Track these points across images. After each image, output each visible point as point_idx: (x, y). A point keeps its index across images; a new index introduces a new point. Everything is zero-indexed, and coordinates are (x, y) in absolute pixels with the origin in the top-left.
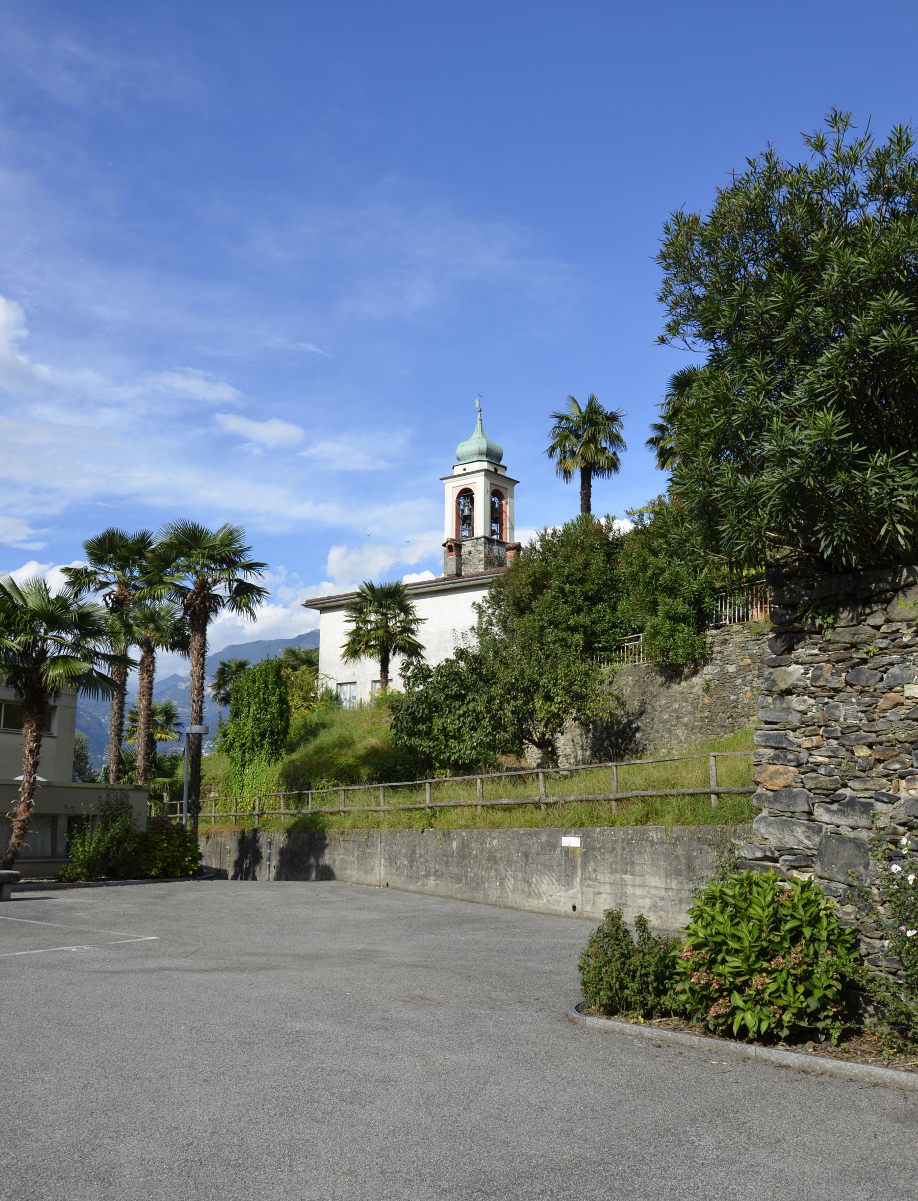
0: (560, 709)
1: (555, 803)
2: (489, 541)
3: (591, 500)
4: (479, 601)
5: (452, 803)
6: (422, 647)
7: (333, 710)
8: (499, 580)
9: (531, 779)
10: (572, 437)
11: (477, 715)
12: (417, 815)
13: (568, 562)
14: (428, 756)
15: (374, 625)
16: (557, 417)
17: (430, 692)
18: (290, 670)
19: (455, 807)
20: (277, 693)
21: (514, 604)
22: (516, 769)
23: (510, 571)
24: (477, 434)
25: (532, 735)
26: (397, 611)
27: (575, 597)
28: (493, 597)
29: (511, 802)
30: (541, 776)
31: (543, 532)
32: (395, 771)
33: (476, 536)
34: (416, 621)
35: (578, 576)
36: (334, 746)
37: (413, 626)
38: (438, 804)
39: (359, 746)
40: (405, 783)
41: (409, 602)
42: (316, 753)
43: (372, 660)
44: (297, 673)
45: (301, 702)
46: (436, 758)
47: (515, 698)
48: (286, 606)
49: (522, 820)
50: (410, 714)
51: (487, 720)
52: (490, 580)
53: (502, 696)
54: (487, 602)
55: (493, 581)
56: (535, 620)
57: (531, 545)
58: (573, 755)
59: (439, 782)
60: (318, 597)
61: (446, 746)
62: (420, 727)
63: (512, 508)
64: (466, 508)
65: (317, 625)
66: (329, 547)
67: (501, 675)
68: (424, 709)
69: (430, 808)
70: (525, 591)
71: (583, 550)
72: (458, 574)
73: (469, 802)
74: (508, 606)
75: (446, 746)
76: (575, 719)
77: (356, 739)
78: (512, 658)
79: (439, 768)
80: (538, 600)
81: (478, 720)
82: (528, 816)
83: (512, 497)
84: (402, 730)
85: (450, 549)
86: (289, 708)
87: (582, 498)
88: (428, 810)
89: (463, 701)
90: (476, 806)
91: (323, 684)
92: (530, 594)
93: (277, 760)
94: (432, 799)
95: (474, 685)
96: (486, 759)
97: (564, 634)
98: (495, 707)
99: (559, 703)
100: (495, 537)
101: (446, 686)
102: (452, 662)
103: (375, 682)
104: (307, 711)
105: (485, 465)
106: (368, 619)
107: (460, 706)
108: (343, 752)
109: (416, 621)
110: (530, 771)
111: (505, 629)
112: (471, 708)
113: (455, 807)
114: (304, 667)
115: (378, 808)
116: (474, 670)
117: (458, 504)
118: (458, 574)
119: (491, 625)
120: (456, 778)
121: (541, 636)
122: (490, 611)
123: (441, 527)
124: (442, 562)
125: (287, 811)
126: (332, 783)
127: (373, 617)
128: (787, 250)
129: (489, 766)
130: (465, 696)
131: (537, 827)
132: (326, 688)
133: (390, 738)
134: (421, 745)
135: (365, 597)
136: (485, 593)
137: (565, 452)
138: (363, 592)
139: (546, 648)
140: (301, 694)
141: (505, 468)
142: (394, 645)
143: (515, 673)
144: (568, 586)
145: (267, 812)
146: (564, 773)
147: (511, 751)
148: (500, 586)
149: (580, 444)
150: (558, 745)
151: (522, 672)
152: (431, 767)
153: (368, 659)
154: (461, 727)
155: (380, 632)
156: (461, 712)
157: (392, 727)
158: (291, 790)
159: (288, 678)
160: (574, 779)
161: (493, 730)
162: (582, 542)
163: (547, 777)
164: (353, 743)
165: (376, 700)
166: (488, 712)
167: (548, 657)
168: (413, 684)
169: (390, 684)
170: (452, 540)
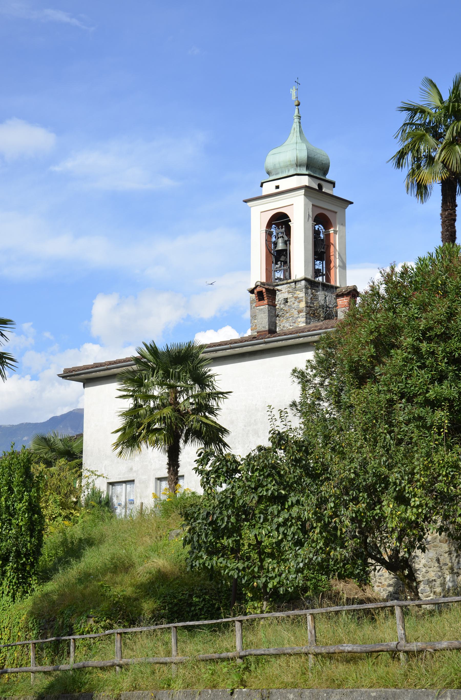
0: (418, 515)
1: (420, 651)
3: (457, 224)
4: (302, 366)
5: (272, 651)
6: (224, 431)
7: (103, 520)
8: (328, 338)
9: (382, 615)
10: (429, 137)
11: (303, 525)
12: (223, 668)
13: (425, 311)
14: (236, 583)
15: (158, 401)
16: (408, 109)
17: (238, 492)
18: (42, 466)
19: (277, 656)
20: (26, 498)
21: (351, 371)
22: (361, 602)
23: (343, 325)
24: (294, 136)
25: (380, 553)
26: (190, 382)
27: (436, 360)
28: (320, 362)
29: (357, 648)
30: (398, 611)
31: (388, 270)
32: (191, 605)
33: (293, 278)
34: (217, 395)
35: (439, 330)
36: (105, 571)
37: (212, 403)
38: (253, 652)
39: (140, 569)
40: (206, 622)
41: (206, 369)
42: (80, 581)
43: (156, 450)
44: (52, 469)
45: (58, 510)
46: (247, 585)
47: (355, 500)
48: (35, 378)
49: (374, 677)
50: (210, 524)
51: (318, 530)
52: (316, 338)
53: (337, 498)
54: (313, 367)
55: (321, 339)
56: (379, 392)
57: (373, 288)
58: (438, 582)
59: (253, 620)
60: (81, 364)
61: (261, 568)
62: (225, 541)
63: (343, 238)
64: (280, 240)
65: (78, 402)
66: (94, 297)
67: (335, 468)
68: (229, 517)
69: (241, 657)
70: (366, 352)
71: (445, 294)
72: (272, 331)
73: (297, 649)
74: (343, 373)
75: (261, 568)
76: (440, 530)
77: (136, 559)
78: (350, 444)
79: (252, 599)
80: (384, 364)
81: (304, 531)
82: (381, 670)
83: (343, 224)
84: (200, 546)
85: (260, 296)
86: (42, 517)
87: (443, 223)
88: (239, 661)
89: (283, 504)
90: (306, 654)
91: (88, 484)
92: (372, 356)
93: (25, 592)
94: (245, 645)
95: (298, 482)
96: (316, 587)
97: (420, 411)
98: (328, 513)
99: (418, 507)
100: (320, 279)
101: (259, 485)
102: (267, 450)
103: (160, 479)
104: (67, 523)
105: (305, 181)
106: (150, 393)
107: (279, 512)
108: (118, 579)
109: (217, 395)
110: (382, 604)
111: (338, 404)
112: (294, 515)
113: (277, 656)
114: (62, 461)
115: (168, 659)
116: (298, 461)
117: (269, 234)
118: (272, 331)
119: (319, 399)
120: (278, 614)
121: (389, 413)
122: (317, 380)
123: (247, 267)
124: (248, 315)
125: (39, 668)
126: (102, 624)
127: (156, 391)
128: (33, 561)
129: (323, 597)
130: (284, 499)
131: (396, 686)
132: (93, 490)
133: (183, 557)
134: (226, 567)
135: (145, 364)
136: (310, 355)
137: (419, 159)
138: (143, 357)
139: (396, 430)
140: (58, 498)
141: (333, 184)
142: (186, 429)
143: (353, 465)
144: (425, 344)
145: (10, 670)
146: (429, 607)
147: (351, 575)
148: (330, 345)
149: (441, 146)
150: (417, 566)
151: (364, 464)
152: (241, 598)
153: (150, 448)
154: (282, 541)
155: (167, 411)
156: (281, 520)
157: (186, 542)
158: (44, 636)
159: (41, 477)
160: (444, 615)
161: (326, 545)
162: (444, 284)
163: (405, 612)
164: (132, 565)
165: (163, 504)
166: (319, 520)
167: (399, 442)
168: (215, 482)
169: (181, 482)
170: (263, 284)
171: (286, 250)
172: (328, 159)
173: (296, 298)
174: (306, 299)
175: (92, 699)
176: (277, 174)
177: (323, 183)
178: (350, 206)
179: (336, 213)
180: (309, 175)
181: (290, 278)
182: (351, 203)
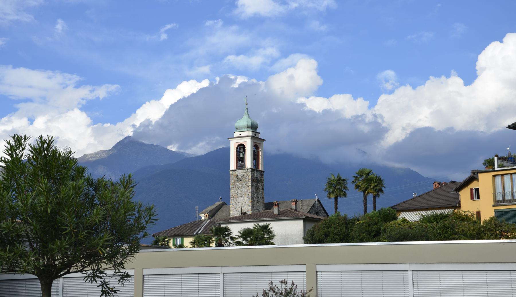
2: (253, 170)
24: (245, 117)
33: (246, 168)
141: (259, 133)
171: (243, 157)
172: (258, 125)
173: (247, 175)
174: (251, 175)
175: (50, 296)
176: (240, 129)
177: (256, 133)
178: (265, 141)
179: (260, 144)
180: (252, 131)
181: (245, 168)
182: (265, 140)
